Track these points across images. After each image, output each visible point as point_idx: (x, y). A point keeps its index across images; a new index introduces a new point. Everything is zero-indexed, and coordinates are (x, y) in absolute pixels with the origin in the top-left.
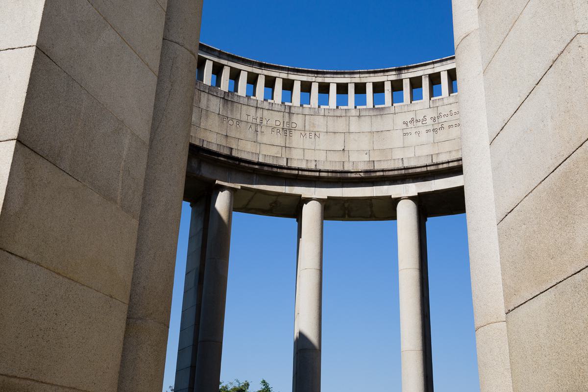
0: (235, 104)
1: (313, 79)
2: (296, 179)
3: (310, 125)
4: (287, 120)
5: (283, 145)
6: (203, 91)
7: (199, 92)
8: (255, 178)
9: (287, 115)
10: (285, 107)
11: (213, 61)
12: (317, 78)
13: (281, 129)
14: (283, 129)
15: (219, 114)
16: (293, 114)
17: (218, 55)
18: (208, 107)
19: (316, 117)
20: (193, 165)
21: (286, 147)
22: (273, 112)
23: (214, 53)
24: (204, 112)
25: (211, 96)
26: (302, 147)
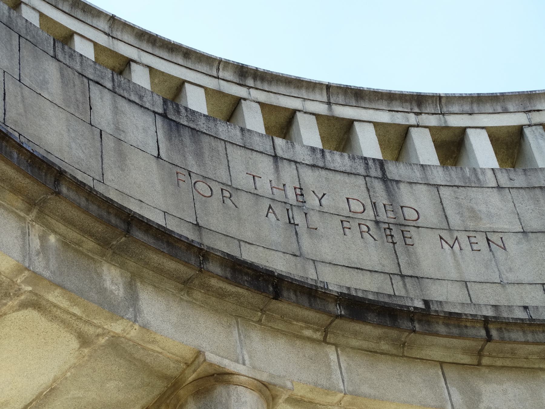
0: (206, 140)
1: (412, 119)
2: (479, 364)
3: (461, 214)
4: (382, 198)
5: (391, 268)
6: (97, 83)
7: (82, 83)
8: (333, 357)
9: (378, 186)
10: (367, 164)
11: (95, 44)
12: (420, 117)
13: (371, 225)
14: (377, 223)
15: (158, 157)
16: (398, 182)
17: (107, 30)
18: (117, 129)
19: (473, 193)
20: (108, 284)
21: (403, 276)
22: (331, 175)
23: (96, 22)
24: (109, 143)
25: (123, 104)
26: (454, 275)
